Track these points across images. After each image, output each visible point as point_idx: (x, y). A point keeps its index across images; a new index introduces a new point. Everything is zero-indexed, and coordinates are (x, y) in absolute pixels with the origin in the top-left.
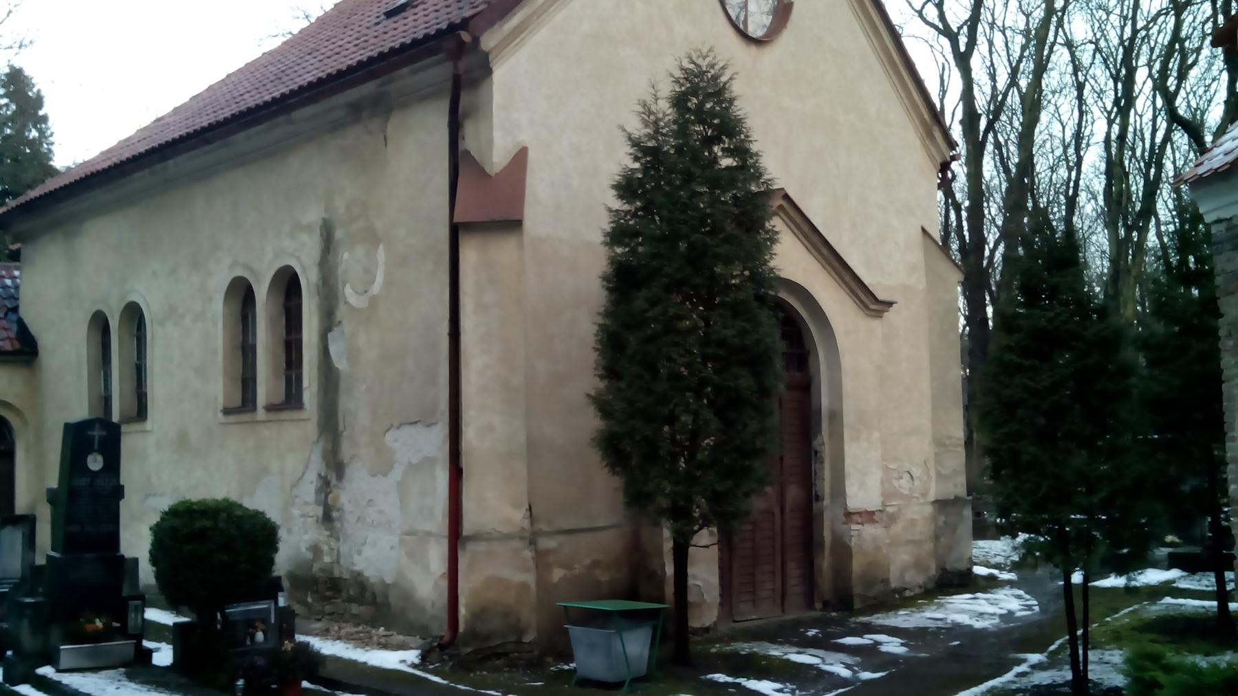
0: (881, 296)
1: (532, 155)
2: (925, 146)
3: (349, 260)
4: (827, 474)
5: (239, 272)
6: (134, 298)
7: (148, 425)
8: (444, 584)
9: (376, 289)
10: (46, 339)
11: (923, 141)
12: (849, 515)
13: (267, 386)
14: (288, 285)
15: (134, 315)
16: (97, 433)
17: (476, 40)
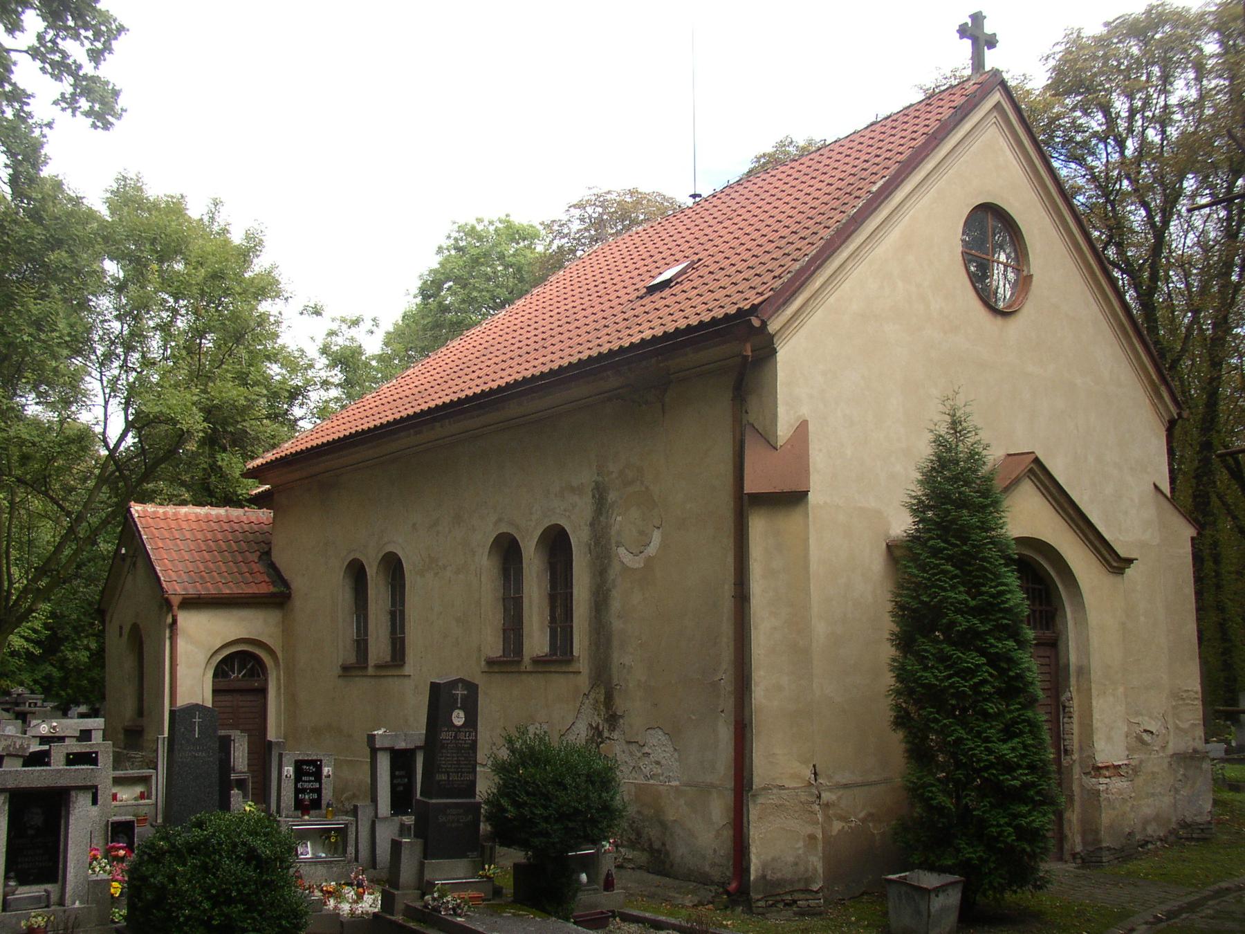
0: (1123, 553)
1: (811, 428)
2: (1154, 405)
3: (623, 522)
4: (1076, 728)
5: (504, 529)
6: (390, 548)
7: (408, 670)
8: (728, 834)
9: (652, 550)
10: (299, 584)
11: (1152, 401)
12: (1098, 770)
13: (537, 641)
14: (556, 543)
15: (393, 567)
16: (460, 692)
17: (764, 324)
